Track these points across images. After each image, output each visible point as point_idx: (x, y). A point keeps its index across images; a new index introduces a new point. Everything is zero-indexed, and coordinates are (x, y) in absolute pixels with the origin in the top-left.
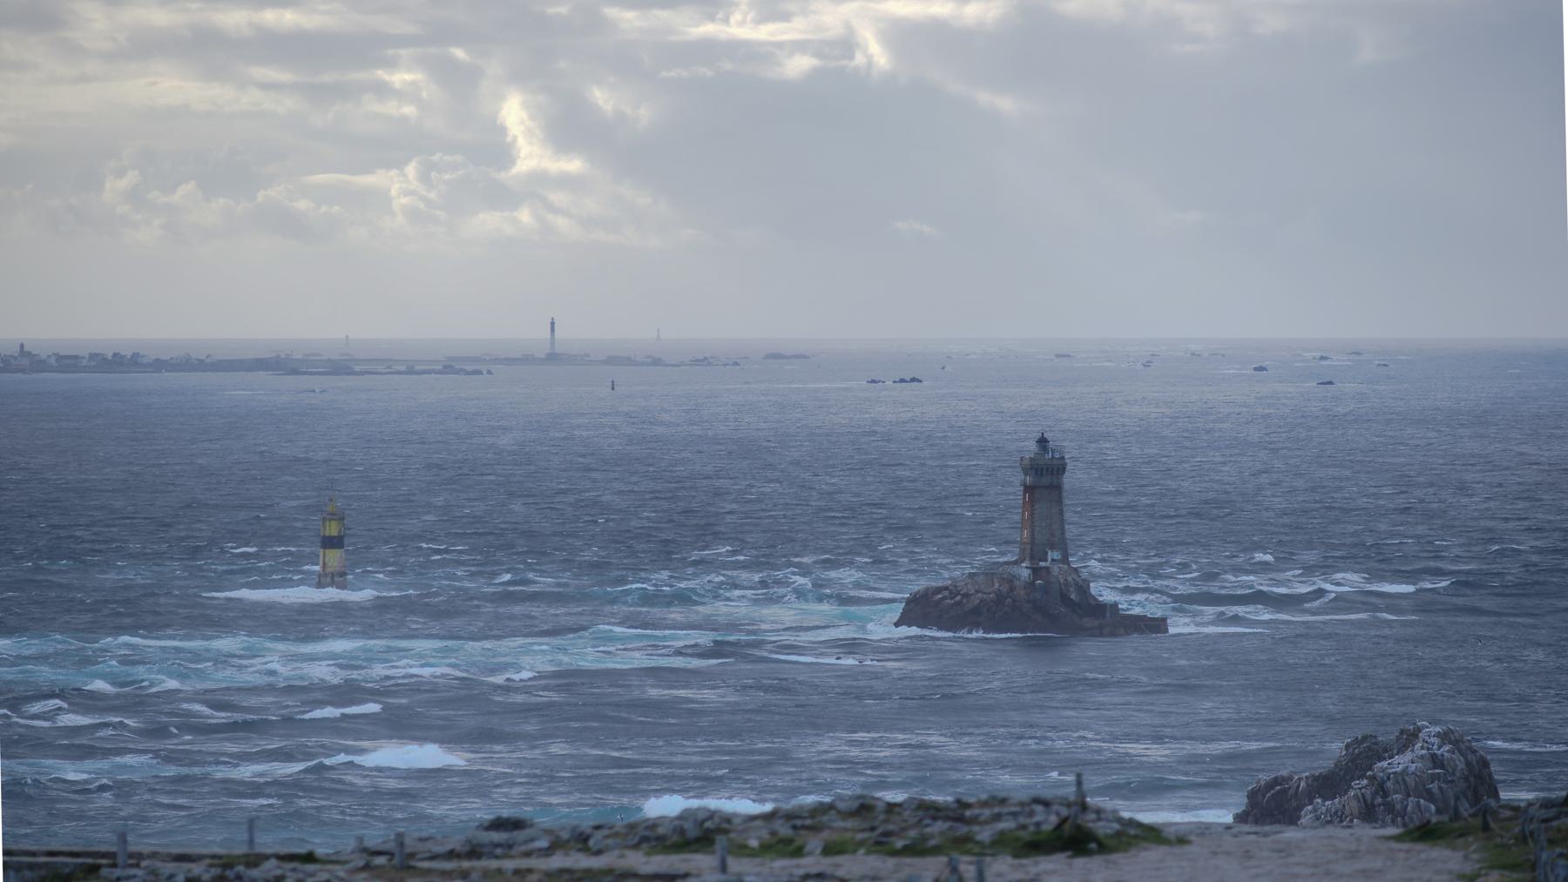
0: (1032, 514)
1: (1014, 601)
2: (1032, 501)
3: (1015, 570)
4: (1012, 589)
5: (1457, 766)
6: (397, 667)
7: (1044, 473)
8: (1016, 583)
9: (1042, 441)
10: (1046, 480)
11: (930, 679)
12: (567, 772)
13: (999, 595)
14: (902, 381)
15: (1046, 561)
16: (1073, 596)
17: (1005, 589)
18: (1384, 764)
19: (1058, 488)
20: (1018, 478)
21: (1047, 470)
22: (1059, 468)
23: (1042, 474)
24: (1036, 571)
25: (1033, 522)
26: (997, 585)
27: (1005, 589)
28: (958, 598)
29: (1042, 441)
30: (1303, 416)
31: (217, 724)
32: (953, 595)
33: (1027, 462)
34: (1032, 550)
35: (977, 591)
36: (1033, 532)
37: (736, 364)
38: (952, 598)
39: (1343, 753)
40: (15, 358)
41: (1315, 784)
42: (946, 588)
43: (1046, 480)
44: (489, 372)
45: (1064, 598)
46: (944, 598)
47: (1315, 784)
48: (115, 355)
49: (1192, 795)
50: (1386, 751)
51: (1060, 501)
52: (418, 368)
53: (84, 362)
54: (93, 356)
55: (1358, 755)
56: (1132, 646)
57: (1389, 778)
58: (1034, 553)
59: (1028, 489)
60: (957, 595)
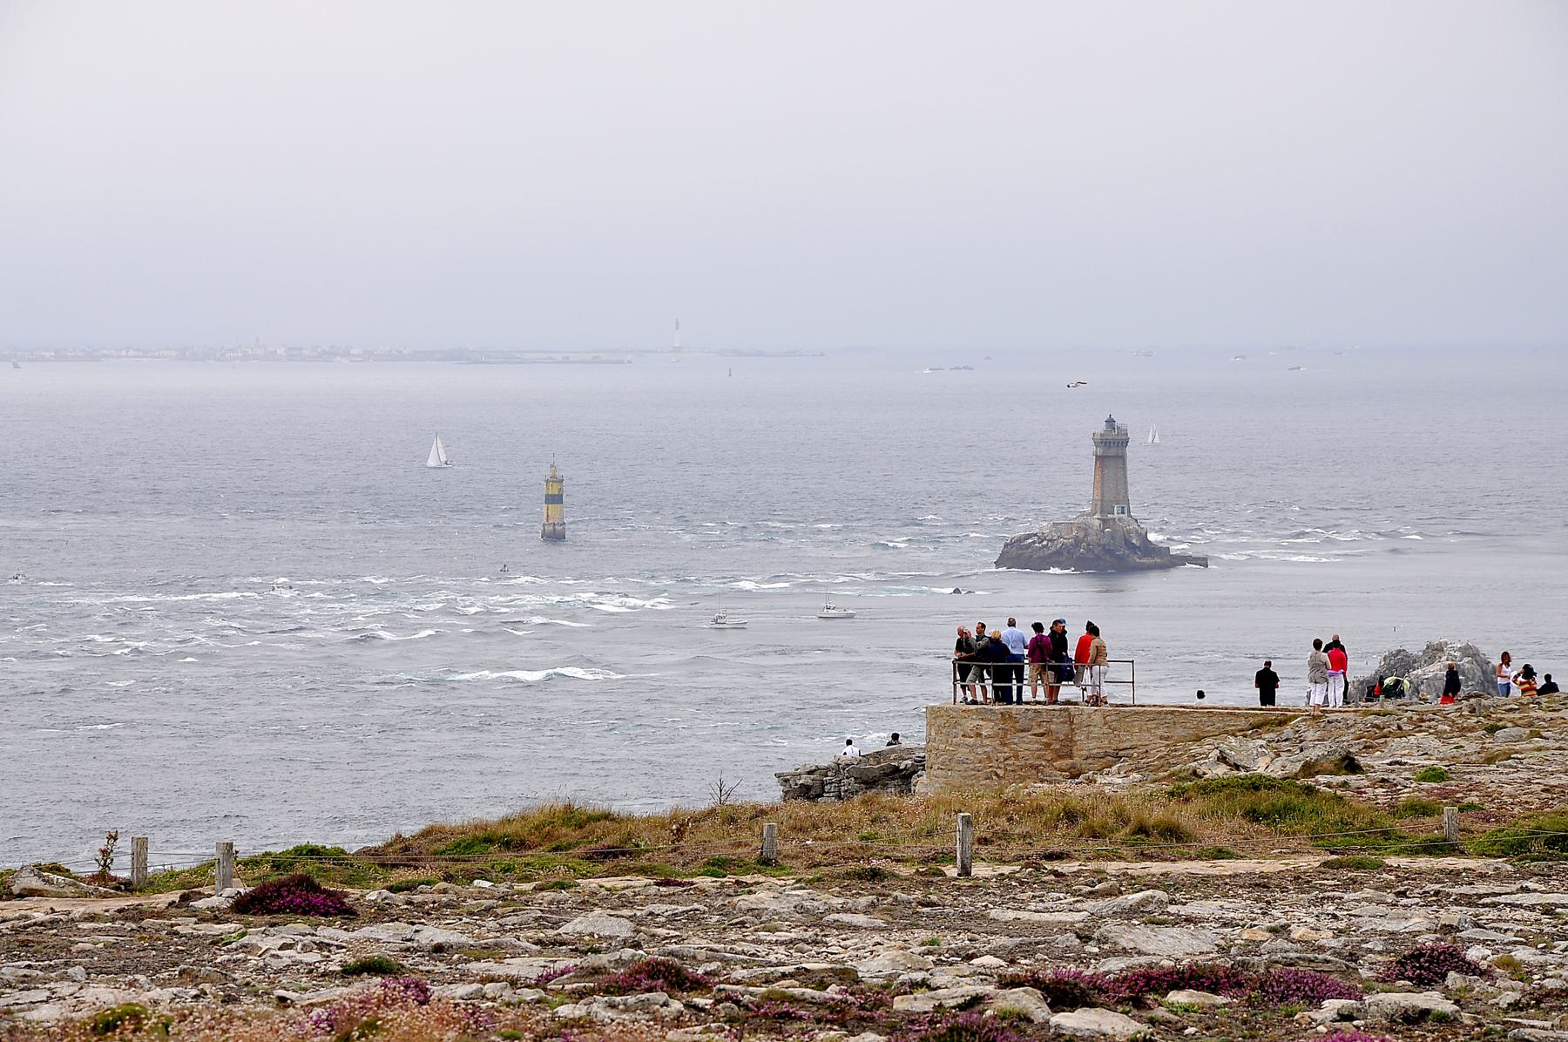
0: (1103, 477)
1: (1089, 545)
3: (1090, 520)
4: (1086, 536)
5: (1475, 674)
6: (1246, 555)
7: (1112, 445)
8: (1090, 531)
10: (1112, 452)
12: (459, 681)
13: (1076, 538)
14: (957, 368)
15: (1113, 514)
16: (1134, 541)
17: (1081, 535)
18: (1419, 671)
19: (1122, 458)
20: (1089, 450)
21: (1114, 443)
23: (1110, 446)
24: (1104, 521)
25: (1103, 484)
27: (1081, 535)
28: (1045, 543)
30: (16, 452)
33: (1099, 437)
34: (1102, 505)
37: (822, 355)
38: (1039, 543)
39: (1383, 663)
41: (1360, 687)
45: (1128, 543)
46: (1034, 542)
47: (1360, 687)
50: (1415, 662)
51: (1124, 468)
55: (1393, 666)
57: (1422, 683)
58: (1104, 507)
59: (1100, 459)
60: (1043, 541)
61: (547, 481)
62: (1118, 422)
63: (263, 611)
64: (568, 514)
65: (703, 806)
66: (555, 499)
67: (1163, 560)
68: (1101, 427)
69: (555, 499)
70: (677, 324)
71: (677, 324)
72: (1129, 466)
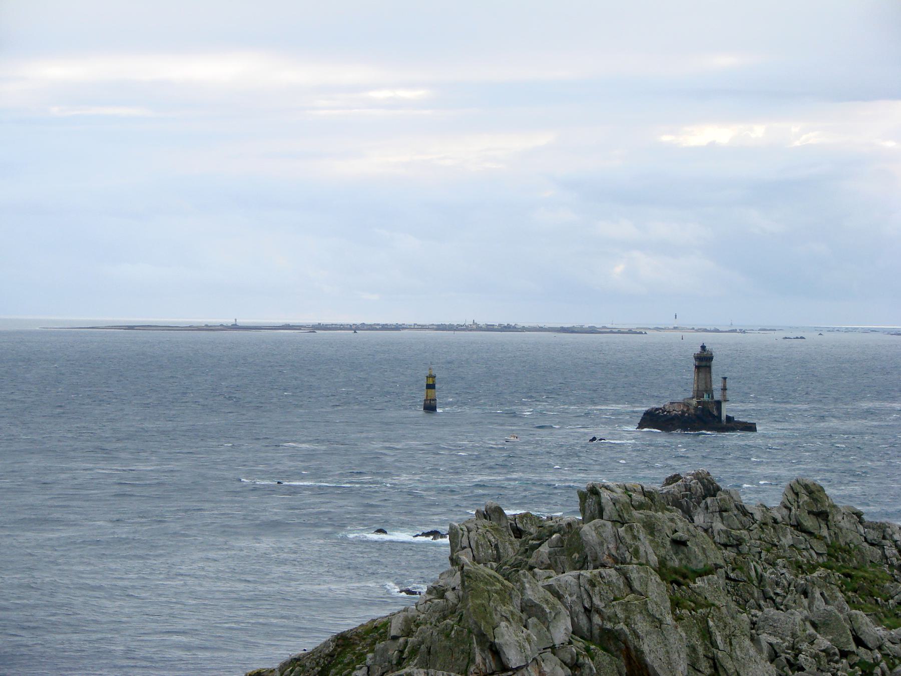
2: (698, 372)
3: (690, 401)
4: (688, 410)
9: (703, 347)
10: (704, 364)
11: (785, 437)
13: (683, 412)
19: (710, 367)
20: (692, 363)
22: (710, 358)
26: (682, 408)
28: (665, 413)
29: (703, 347)
31: (654, 428)
32: (663, 411)
35: (674, 410)
36: (698, 386)
40: (471, 325)
42: (661, 409)
43: (704, 364)
44: (646, 333)
48: (508, 324)
49: (321, 636)
51: (710, 372)
52: (614, 330)
53: (496, 327)
54: (500, 325)
56: (734, 438)
59: (697, 367)
61: (427, 377)
62: (707, 348)
63: (203, 569)
64: (438, 394)
65: (462, 324)
66: (430, 387)
67: (731, 425)
68: (698, 350)
69: (430, 387)
70: (676, 316)
71: (676, 316)
72: (713, 370)
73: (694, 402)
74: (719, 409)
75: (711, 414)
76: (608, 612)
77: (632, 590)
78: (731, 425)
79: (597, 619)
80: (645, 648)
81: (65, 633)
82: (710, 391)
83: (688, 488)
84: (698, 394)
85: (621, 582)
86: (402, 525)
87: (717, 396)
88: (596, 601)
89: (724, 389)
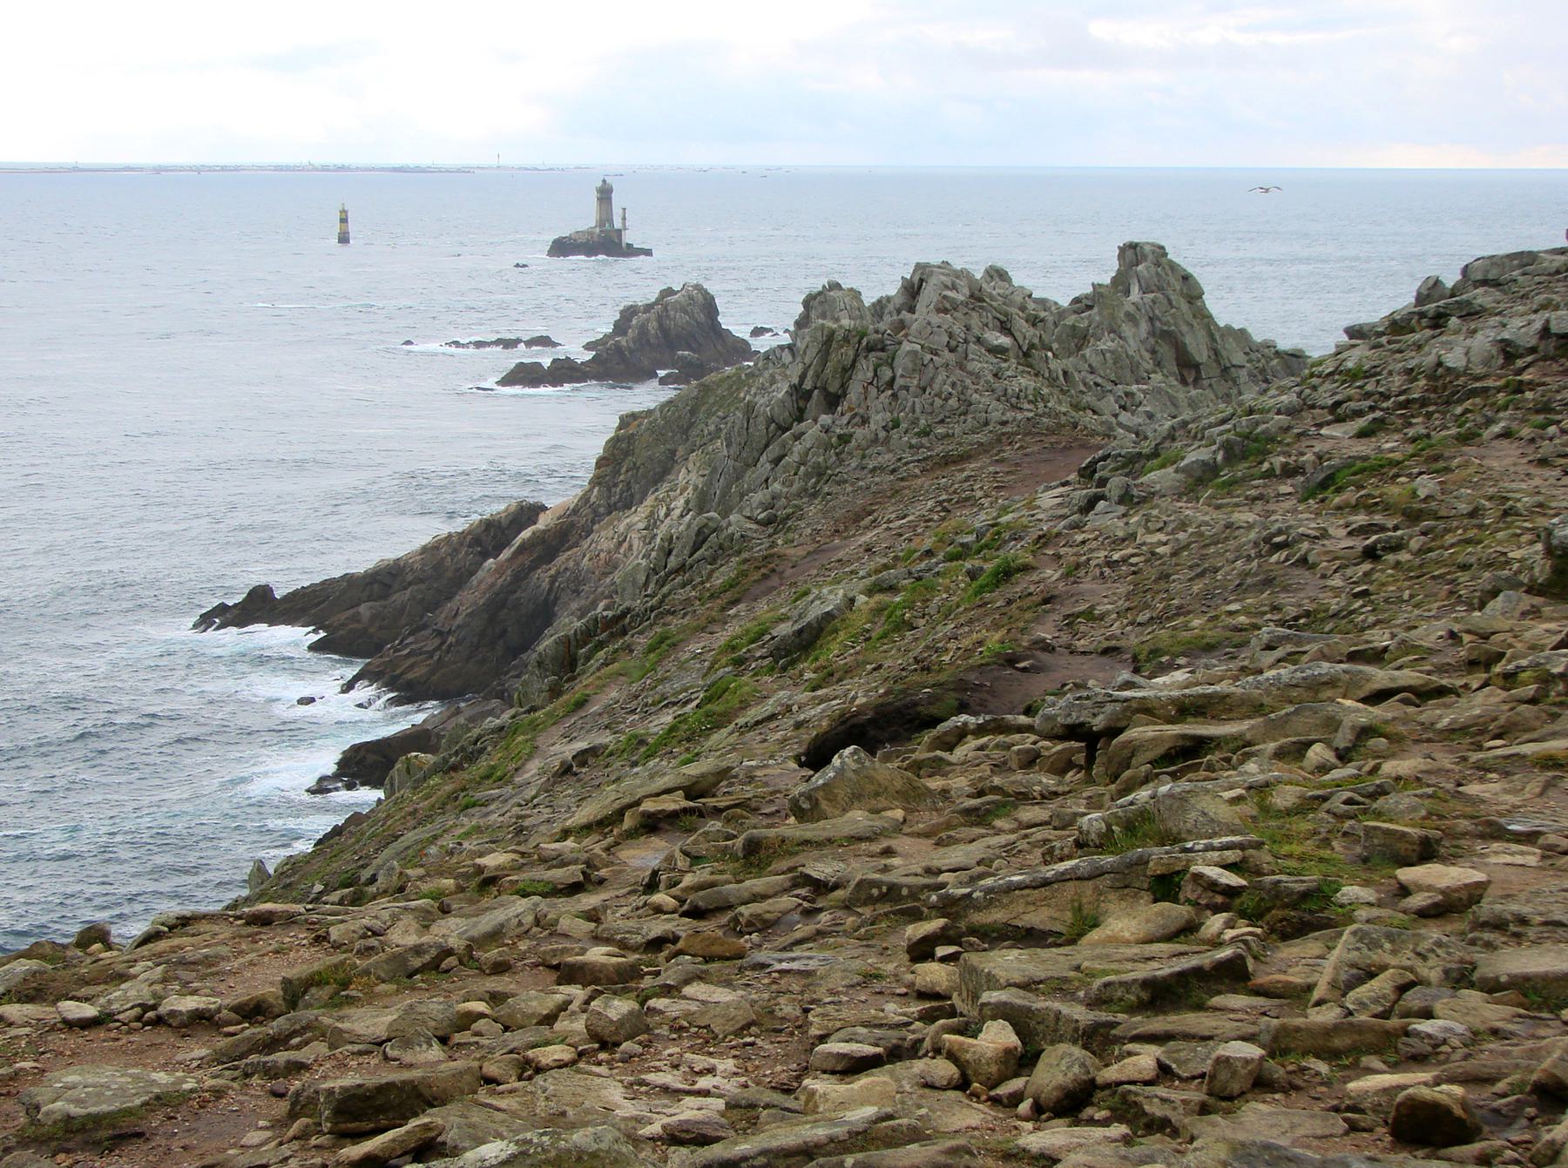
9: (604, 181)
29: (604, 181)
64: (352, 228)
66: (344, 221)
67: (631, 251)
68: (599, 184)
69: (344, 221)
73: (598, 230)
74: (620, 236)
75: (613, 241)
76: (1164, 319)
77: (1172, 307)
78: (631, 251)
79: (1158, 324)
80: (1187, 341)
81: (478, 388)
82: (611, 221)
83: (691, 298)
84: (601, 223)
85: (1166, 301)
86: (427, 338)
87: (618, 224)
88: (1157, 312)
89: (624, 219)
